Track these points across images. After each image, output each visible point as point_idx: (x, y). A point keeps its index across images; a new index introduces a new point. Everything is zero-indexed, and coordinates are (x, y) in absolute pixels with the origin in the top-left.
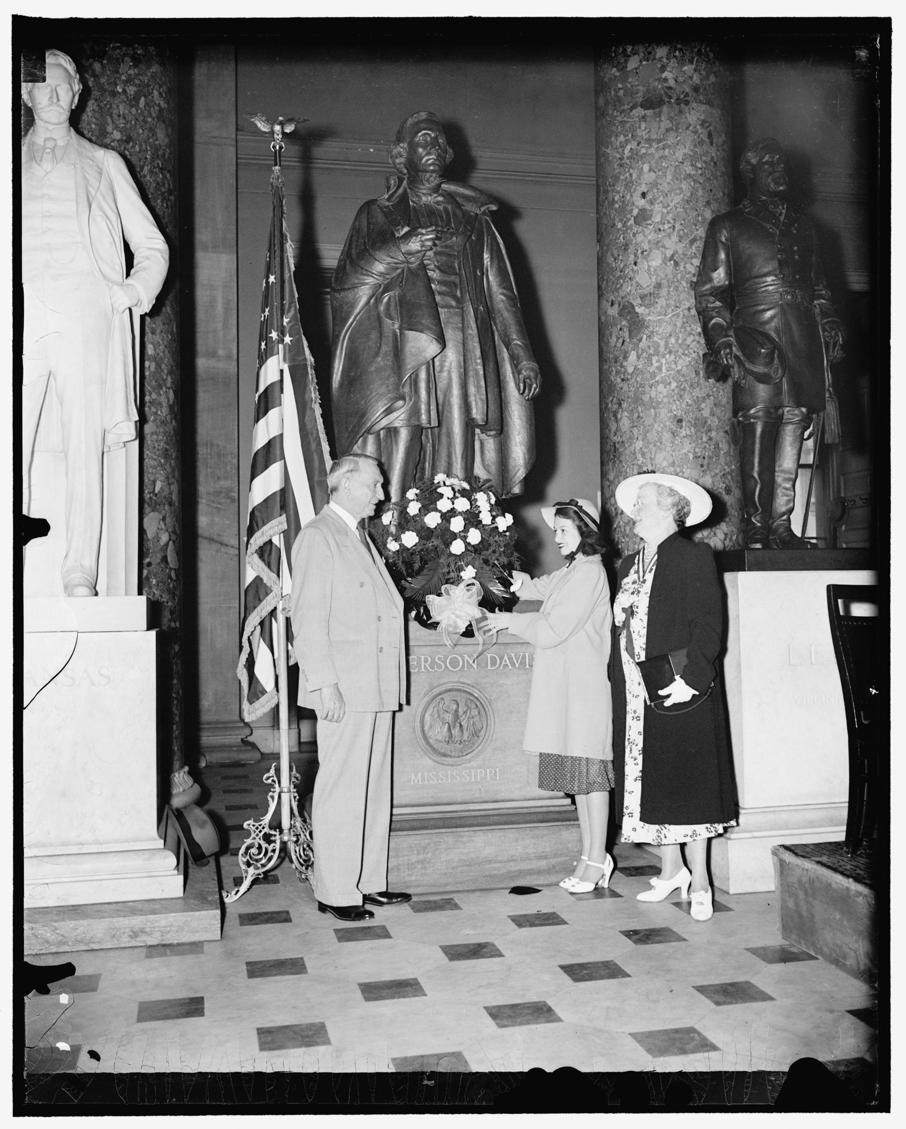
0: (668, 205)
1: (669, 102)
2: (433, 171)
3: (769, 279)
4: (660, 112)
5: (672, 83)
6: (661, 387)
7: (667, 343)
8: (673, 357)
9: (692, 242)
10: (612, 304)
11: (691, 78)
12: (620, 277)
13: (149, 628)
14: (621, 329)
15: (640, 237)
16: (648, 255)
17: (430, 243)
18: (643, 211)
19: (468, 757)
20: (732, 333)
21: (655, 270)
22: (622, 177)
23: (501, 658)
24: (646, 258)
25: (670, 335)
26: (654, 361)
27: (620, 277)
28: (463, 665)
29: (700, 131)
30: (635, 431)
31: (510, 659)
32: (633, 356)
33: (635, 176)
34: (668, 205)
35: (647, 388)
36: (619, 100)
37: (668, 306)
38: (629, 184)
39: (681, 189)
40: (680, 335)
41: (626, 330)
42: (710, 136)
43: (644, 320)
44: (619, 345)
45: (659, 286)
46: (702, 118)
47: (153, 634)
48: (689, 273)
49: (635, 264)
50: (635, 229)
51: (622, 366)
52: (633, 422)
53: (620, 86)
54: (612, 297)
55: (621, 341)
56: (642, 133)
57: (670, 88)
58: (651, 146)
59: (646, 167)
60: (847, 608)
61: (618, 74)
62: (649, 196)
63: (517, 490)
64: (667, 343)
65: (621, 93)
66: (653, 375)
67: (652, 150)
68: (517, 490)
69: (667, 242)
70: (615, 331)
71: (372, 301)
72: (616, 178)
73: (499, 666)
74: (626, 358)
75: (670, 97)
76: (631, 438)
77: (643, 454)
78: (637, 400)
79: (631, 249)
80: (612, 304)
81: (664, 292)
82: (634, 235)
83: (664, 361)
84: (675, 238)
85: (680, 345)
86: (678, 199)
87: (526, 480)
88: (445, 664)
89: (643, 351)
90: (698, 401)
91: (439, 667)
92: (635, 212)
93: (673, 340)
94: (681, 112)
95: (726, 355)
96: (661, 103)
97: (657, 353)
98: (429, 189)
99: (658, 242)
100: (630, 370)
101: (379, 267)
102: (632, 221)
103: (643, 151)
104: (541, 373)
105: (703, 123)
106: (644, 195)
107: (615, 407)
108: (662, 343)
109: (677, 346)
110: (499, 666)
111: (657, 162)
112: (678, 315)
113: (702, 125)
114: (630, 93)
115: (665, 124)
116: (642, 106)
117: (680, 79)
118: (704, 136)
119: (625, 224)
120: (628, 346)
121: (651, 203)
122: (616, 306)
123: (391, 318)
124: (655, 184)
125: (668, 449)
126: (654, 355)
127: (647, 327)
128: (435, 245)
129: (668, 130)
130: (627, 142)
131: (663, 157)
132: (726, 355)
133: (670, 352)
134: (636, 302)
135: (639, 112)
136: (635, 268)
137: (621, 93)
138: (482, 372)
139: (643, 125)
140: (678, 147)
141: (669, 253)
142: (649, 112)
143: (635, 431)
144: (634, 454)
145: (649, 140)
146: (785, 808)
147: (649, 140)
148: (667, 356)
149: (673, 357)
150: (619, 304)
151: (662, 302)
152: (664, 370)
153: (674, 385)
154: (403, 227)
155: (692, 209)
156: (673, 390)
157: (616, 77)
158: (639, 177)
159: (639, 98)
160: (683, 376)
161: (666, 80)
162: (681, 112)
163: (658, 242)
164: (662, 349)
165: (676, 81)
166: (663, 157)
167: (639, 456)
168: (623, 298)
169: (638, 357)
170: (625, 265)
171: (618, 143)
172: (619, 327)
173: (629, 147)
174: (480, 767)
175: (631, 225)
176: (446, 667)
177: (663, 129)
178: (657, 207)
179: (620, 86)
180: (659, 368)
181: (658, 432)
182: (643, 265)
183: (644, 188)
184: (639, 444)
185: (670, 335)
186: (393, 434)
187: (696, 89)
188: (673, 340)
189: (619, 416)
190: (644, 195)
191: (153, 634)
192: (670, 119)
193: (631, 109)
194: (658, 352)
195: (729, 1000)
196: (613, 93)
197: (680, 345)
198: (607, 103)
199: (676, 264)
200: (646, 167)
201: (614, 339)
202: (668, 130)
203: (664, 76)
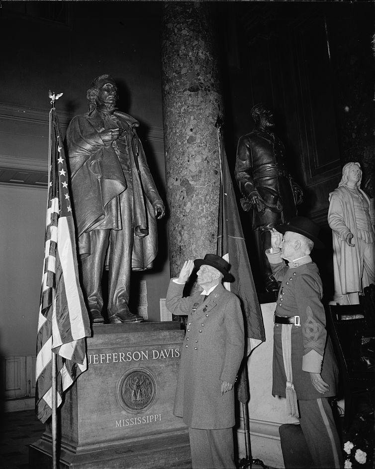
0: (203, 135)
1: (202, 90)
2: (112, 103)
4: (198, 93)
6: (203, 219)
7: (205, 198)
8: (208, 205)
9: (215, 152)
10: (177, 180)
11: (210, 80)
12: (181, 167)
14: (182, 192)
15: (190, 149)
16: (195, 157)
17: (116, 137)
18: (191, 137)
19: (145, 409)
20: (256, 189)
21: (198, 165)
22: (180, 122)
23: (160, 353)
25: (207, 195)
26: (200, 207)
27: (181, 167)
28: (141, 357)
29: (215, 104)
30: (191, 240)
31: (164, 352)
32: (189, 204)
33: (187, 121)
34: (203, 135)
35: (197, 220)
36: (177, 87)
37: (205, 181)
38: (184, 125)
39: (208, 128)
40: (212, 195)
41: (185, 192)
42: (219, 106)
43: (194, 187)
44: (181, 199)
45: (200, 172)
46: (216, 98)
48: (214, 166)
49: (189, 161)
51: (183, 209)
52: (190, 236)
53: (178, 81)
54: (176, 177)
55: (182, 197)
56: (190, 102)
57: (202, 83)
58: (194, 108)
59: (192, 118)
60: (340, 318)
61: (176, 75)
62: (194, 131)
63: (149, 266)
64: (205, 198)
65: (178, 84)
66: (200, 213)
68: (149, 266)
70: (179, 193)
71: (85, 164)
73: (159, 357)
74: (185, 205)
75: (202, 87)
76: (189, 243)
77: (196, 251)
78: (192, 225)
79: (186, 154)
80: (177, 180)
81: (203, 174)
82: (187, 148)
83: (204, 207)
84: (207, 150)
85: (212, 199)
86: (207, 133)
87: (154, 262)
88: (132, 357)
89: (194, 202)
91: (129, 359)
92: (188, 137)
93: (208, 197)
94: (207, 94)
95: (256, 199)
96: (197, 90)
97: (201, 203)
98: (109, 112)
99: (199, 152)
100: (188, 211)
101: (88, 147)
103: (191, 110)
104: (355, 162)
105: (216, 100)
107: (180, 229)
108: (203, 198)
109: (210, 200)
110: (159, 357)
111: (197, 115)
112: (210, 186)
113: (216, 101)
114: (183, 84)
115: (200, 99)
116: (189, 90)
117: (206, 80)
118: (217, 106)
120: (186, 199)
122: (179, 181)
123: (95, 173)
125: (208, 249)
126: (199, 204)
127: (196, 191)
128: (118, 138)
131: (201, 114)
132: (256, 199)
133: (207, 203)
134: (190, 179)
135: (188, 92)
136: (188, 163)
137: (178, 84)
138: (143, 202)
139: (190, 99)
140: (206, 110)
141: (204, 157)
142: (192, 93)
143: (191, 240)
144: (191, 251)
145: (193, 106)
146: (261, 422)
147: (193, 106)
148: (206, 204)
149: (208, 205)
150: (181, 180)
151: (202, 179)
152: (205, 211)
153: (210, 218)
154: (101, 128)
155: (214, 137)
156: (209, 221)
157: (175, 77)
158: (189, 122)
159: (188, 87)
160: (213, 214)
161: (200, 80)
162: (207, 94)
163: (199, 152)
164: (203, 201)
165: (204, 80)
166: (201, 114)
167: (194, 252)
168: (182, 177)
169: (192, 205)
170: (183, 162)
171: (177, 106)
172: (181, 190)
173: (183, 108)
174: (151, 414)
175: (186, 144)
176: (132, 358)
177: (199, 101)
178: (198, 136)
179: (178, 81)
180: (202, 210)
181: (203, 241)
182: (192, 162)
184: (194, 246)
185: (207, 195)
186: (97, 233)
187: (212, 85)
188: (208, 197)
189: (182, 233)
192: (202, 97)
193: (184, 91)
194: (202, 202)
196: (174, 84)
197: (212, 199)
198: (170, 88)
199: (208, 162)
200: (192, 118)
201: (178, 196)
202: (202, 102)
203: (199, 77)
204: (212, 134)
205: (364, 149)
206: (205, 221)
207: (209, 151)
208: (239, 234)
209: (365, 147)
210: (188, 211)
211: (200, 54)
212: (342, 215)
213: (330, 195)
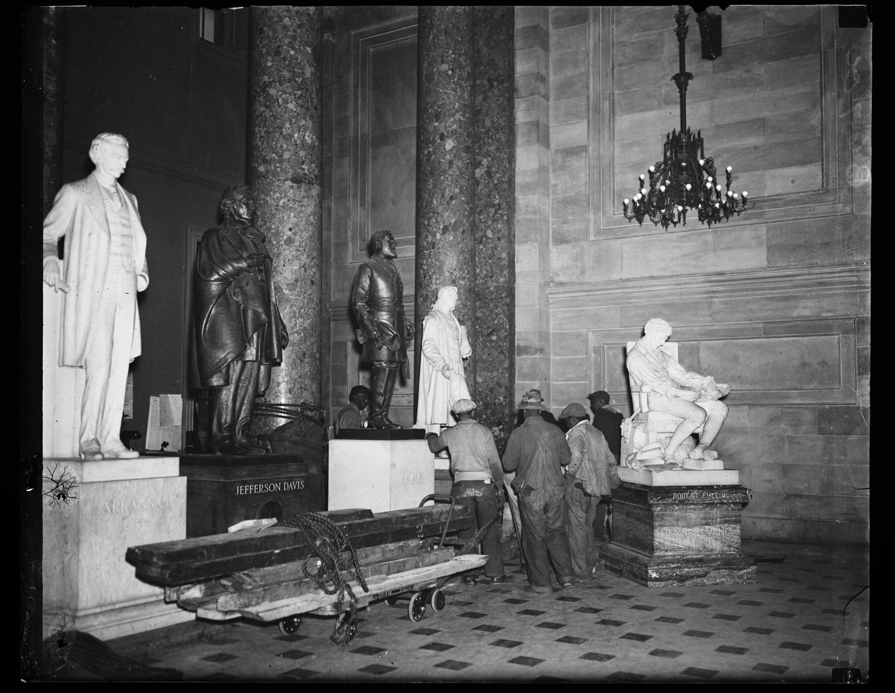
3: (230, 268)
5: (306, 172)
9: (312, 259)
13: (182, 474)
15: (287, 252)
24: (291, 264)
33: (285, 218)
38: (281, 221)
47: (185, 479)
50: (285, 247)
59: (292, 215)
62: (293, 231)
67: (296, 206)
69: (302, 258)
72: (273, 216)
81: (299, 284)
84: (305, 256)
90: (312, 344)
92: (285, 237)
102: (283, 242)
106: (290, 229)
108: (297, 311)
115: (303, 193)
119: (278, 242)
121: (295, 234)
124: (297, 225)
129: (304, 197)
130: (281, 198)
139: (291, 191)
142: (295, 185)
145: (294, 200)
147: (294, 200)
158: (288, 219)
161: (304, 169)
173: (282, 201)
178: (297, 237)
183: (290, 226)
190: (290, 229)
191: (185, 479)
192: (305, 191)
193: (285, 180)
195: (289, 676)
199: (306, 270)
202: (304, 197)
207: (308, 257)
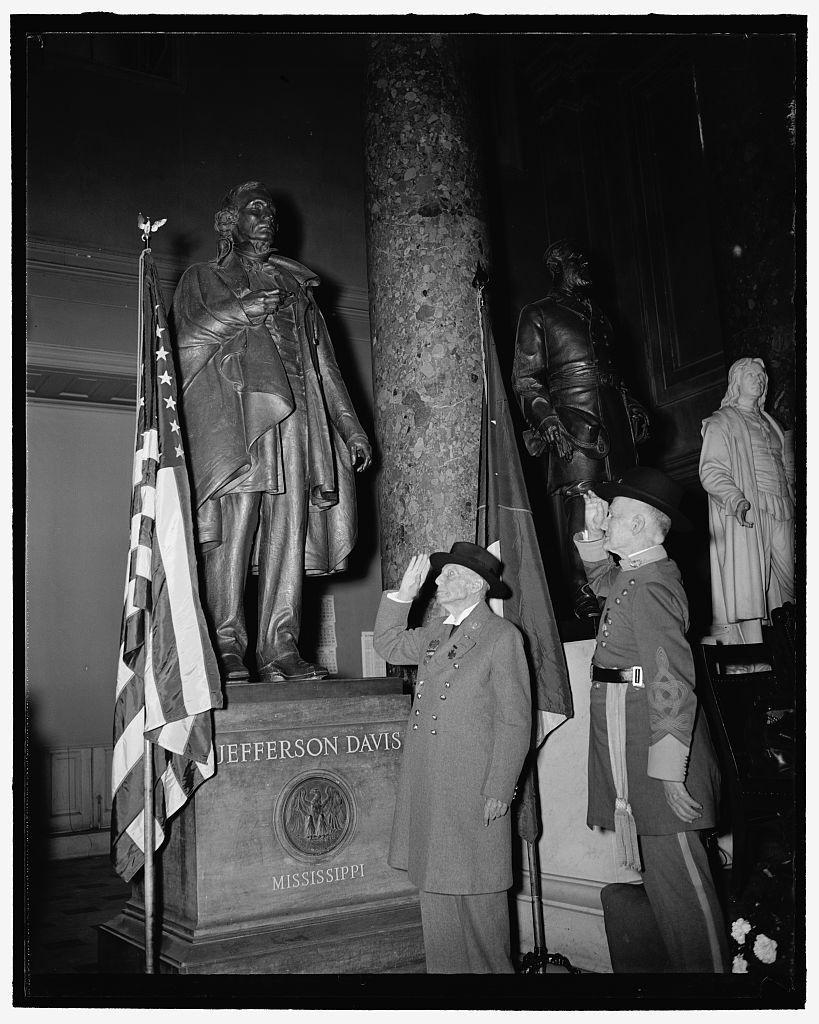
0: (449, 304)
1: (446, 212)
2: (265, 240)
4: (438, 220)
6: (449, 472)
7: (453, 430)
8: (459, 443)
9: (471, 338)
10: (395, 393)
11: (463, 193)
12: (403, 368)
14: (405, 417)
15: (422, 332)
16: (431, 348)
17: (274, 307)
18: (424, 307)
19: (331, 853)
20: (554, 412)
21: (439, 363)
22: (402, 276)
23: (361, 741)
25: (456, 423)
26: (441, 447)
27: (403, 368)
28: (324, 749)
29: (473, 240)
30: (425, 514)
31: (370, 740)
32: (420, 443)
33: (415, 276)
34: (449, 304)
35: (436, 473)
36: (397, 206)
37: (453, 396)
38: (409, 283)
39: (459, 289)
40: (465, 424)
41: (412, 418)
42: (480, 245)
43: (430, 408)
44: (404, 432)
45: (443, 377)
46: (473, 228)
48: (470, 366)
49: (419, 356)
51: (408, 452)
52: (422, 506)
53: (397, 194)
54: (394, 387)
55: (406, 428)
56: (421, 236)
57: (446, 199)
58: (430, 250)
59: (426, 268)
60: (723, 670)
61: (395, 183)
62: (430, 295)
63: (341, 566)
64: (453, 430)
65: (399, 200)
66: (442, 460)
68: (341, 566)
70: (399, 419)
71: (210, 361)
73: (360, 749)
74: (412, 444)
75: (446, 208)
76: (421, 521)
77: (434, 537)
78: (426, 484)
79: (414, 342)
80: (395, 393)
81: (448, 382)
82: (417, 329)
83: (451, 447)
84: (456, 334)
85: (465, 433)
86: (456, 299)
87: (349, 558)
88: (305, 749)
89: (430, 438)
91: (300, 752)
92: (417, 308)
93: (458, 428)
94: (456, 221)
95: (554, 432)
96: (437, 212)
97: (444, 439)
98: (259, 257)
99: (440, 337)
100: (418, 455)
101: (217, 326)
103: (423, 253)
104: (754, 358)
105: (475, 233)
107: (402, 491)
108: (448, 430)
109: (462, 434)
110: (360, 749)
111: (436, 263)
112: (461, 405)
113: (474, 235)
114: (409, 201)
115: (443, 230)
116: (420, 213)
117: (454, 193)
118: (476, 245)
120: (414, 432)
122: (400, 395)
123: (232, 379)
125: (459, 531)
126: (441, 442)
127: (433, 415)
128: (277, 309)
131: (443, 260)
132: (554, 432)
133: (457, 439)
134: (421, 392)
135: (417, 218)
136: (419, 360)
137: (399, 200)
138: (328, 439)
139: (422, 230)
140: (455, 252)
141: (451, 348)
142: (426, 219)
143: (425, 514)
144: (425, 536)
145: (428, 244)
147: (428, 244)
148: (454, 443)
149: (459, 443)
150: (403, 394)
151: (447, 392)
152: (451, 456)
153: (461, 470)
154: (243, 289)
155: (470, 308)
156: (461, 475)
157: (392, 186)
158: (420, 276)
159: (417, 206)
160: (469, 462)
161: (441, 192)
162: (456, 221)
163: (440, 337)
164: (449, 436)
165: (450, 194)
166: (443, 260)
167: (429, 538)
168: (406, 387)
169: (426, 443)
170: (408, 357)
171: (397, 245)
172: (404, 415)
173: (408, 249)
174: (344, 864)
175: (414, 321)
176: (306, 752)
177: (440, 236)
178: (439, 305)
179: (397, 194)
180: (447, 454)
181: (448, 515)
182: (427, 357)
184: (430, 527)
185: (456, 423)
186: (234, 501)
187: (467, 203)
188: (458, 428)
189: (407, 501)
192: (447, 226)
193: (409, 216)
194: (445, 439)
196: (390, 200)
197: (465, 433)
198: (382, 210)
199: (458, 358)
200: (426, 268)
201: (398, 426)
202: (445, 236)
203: (440, 187)
204: (466, 302)
205: (773, 332)
206: (453, 476)
207: (461, 335)
208: (521, 503)
209: (774, 328)
210: (418, 455)
211: (442, 141)
212: (727, 464)
213: (704, 423)
